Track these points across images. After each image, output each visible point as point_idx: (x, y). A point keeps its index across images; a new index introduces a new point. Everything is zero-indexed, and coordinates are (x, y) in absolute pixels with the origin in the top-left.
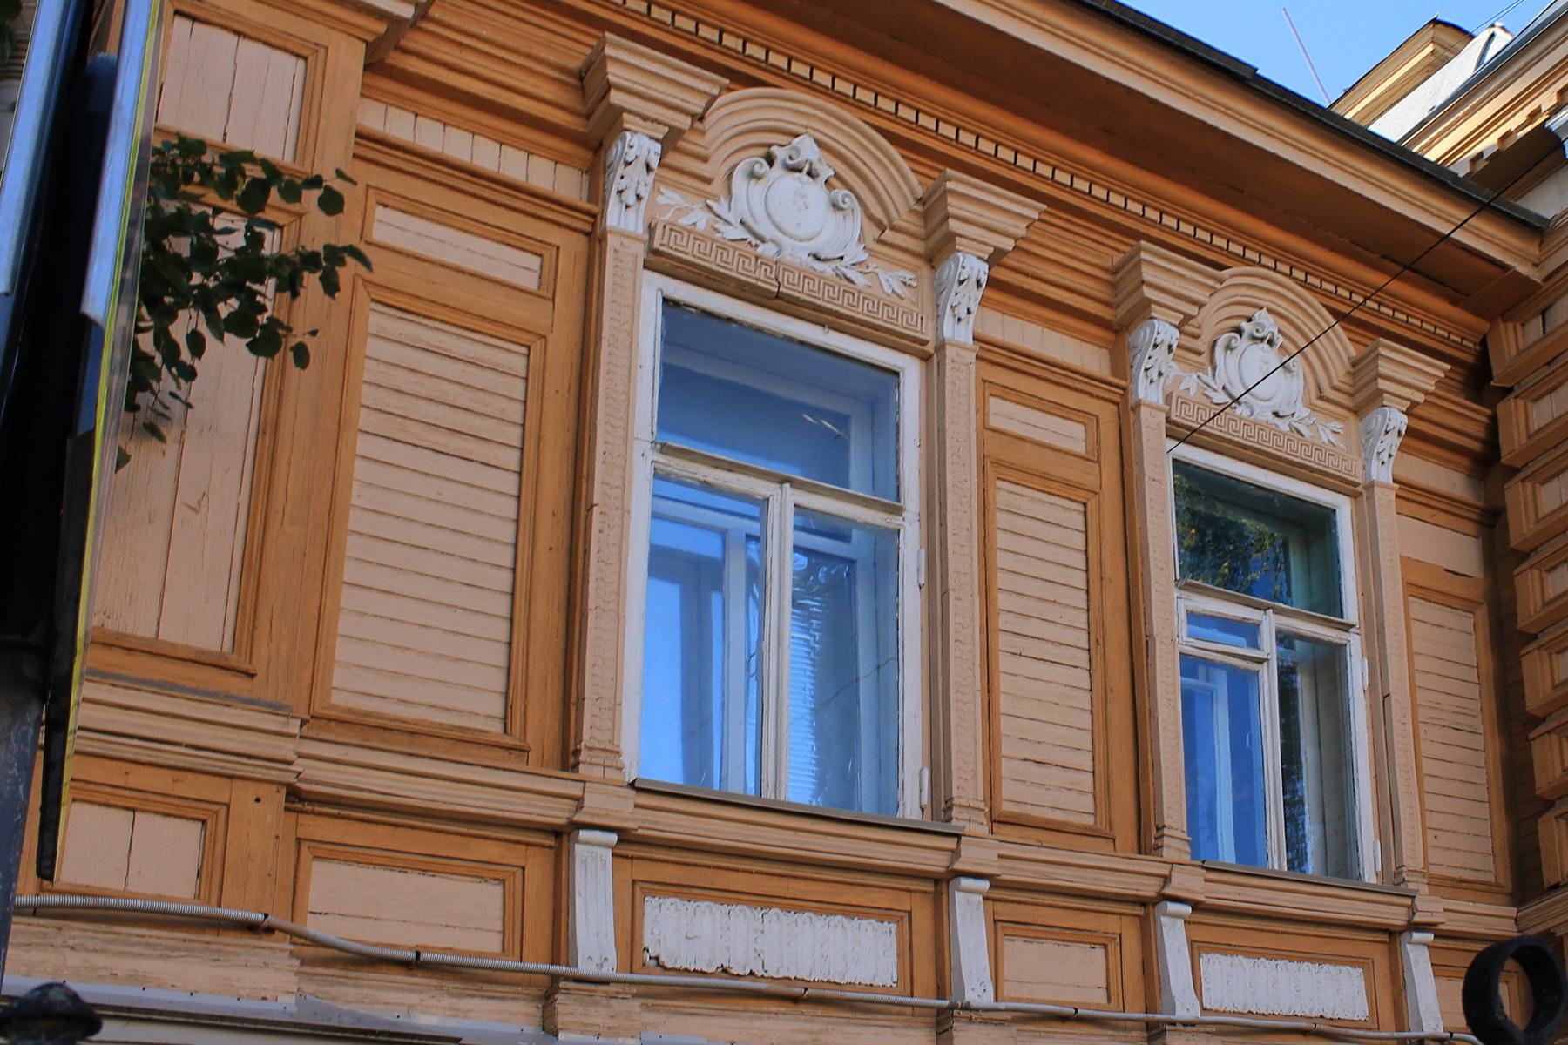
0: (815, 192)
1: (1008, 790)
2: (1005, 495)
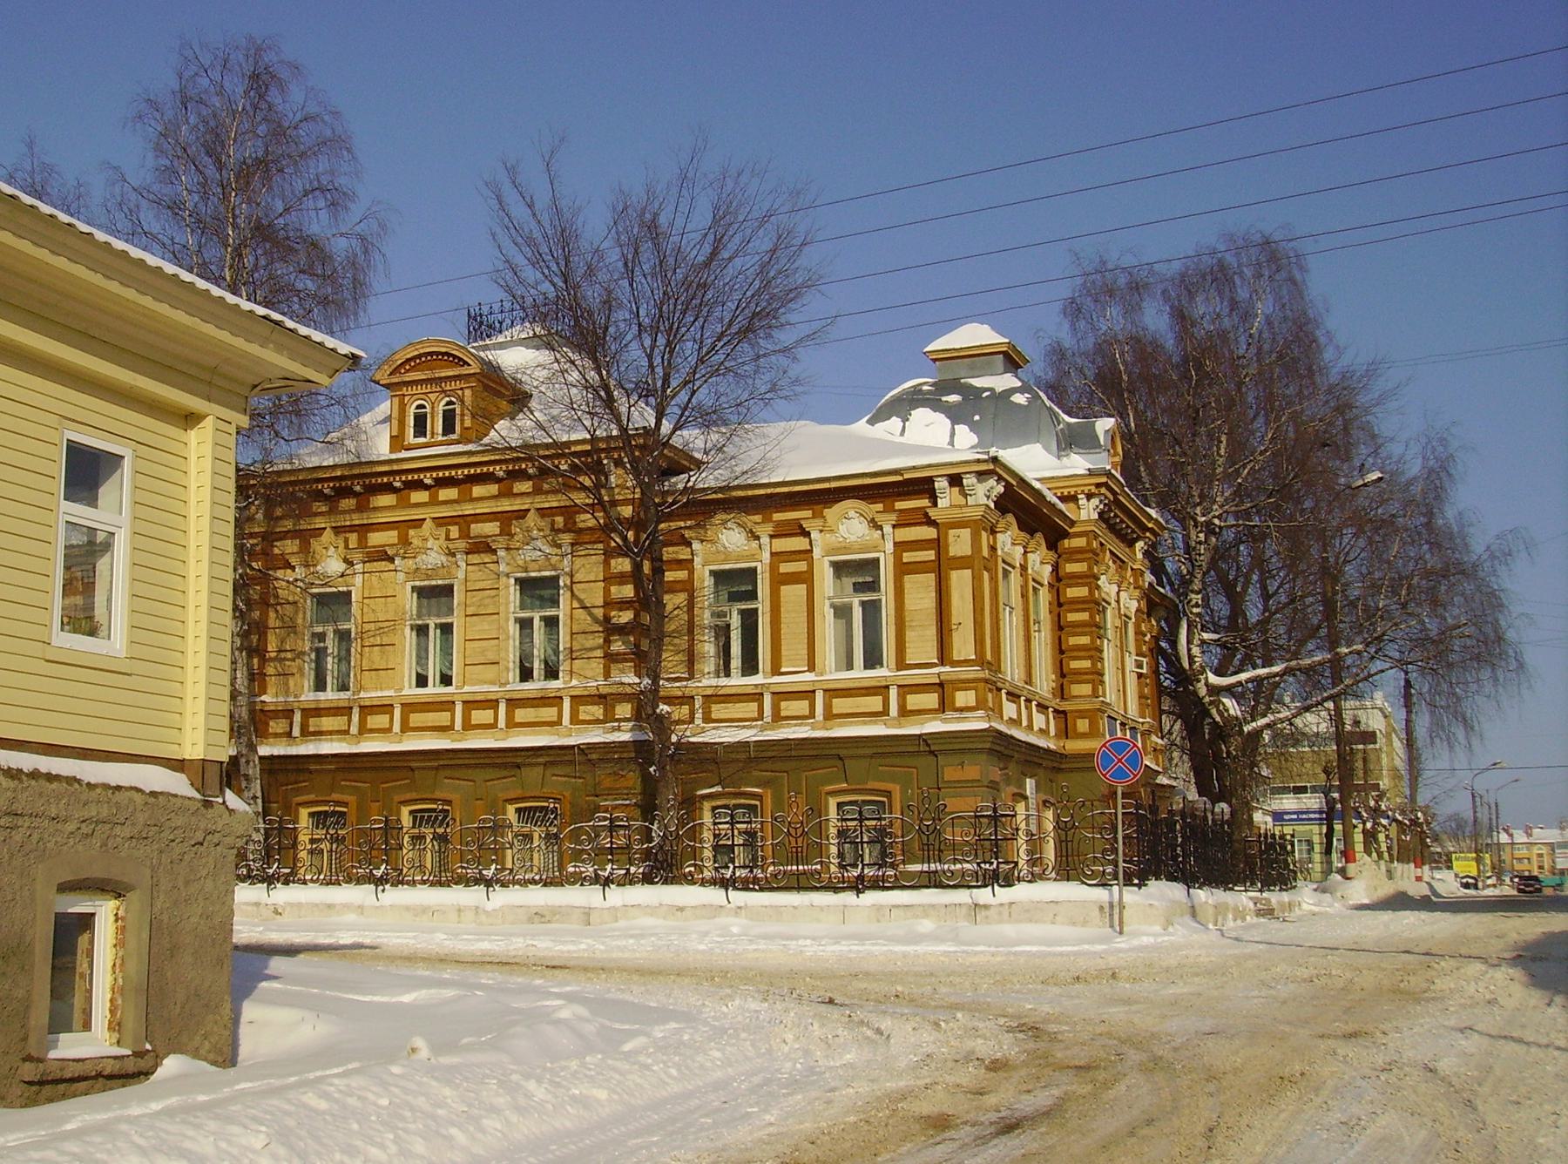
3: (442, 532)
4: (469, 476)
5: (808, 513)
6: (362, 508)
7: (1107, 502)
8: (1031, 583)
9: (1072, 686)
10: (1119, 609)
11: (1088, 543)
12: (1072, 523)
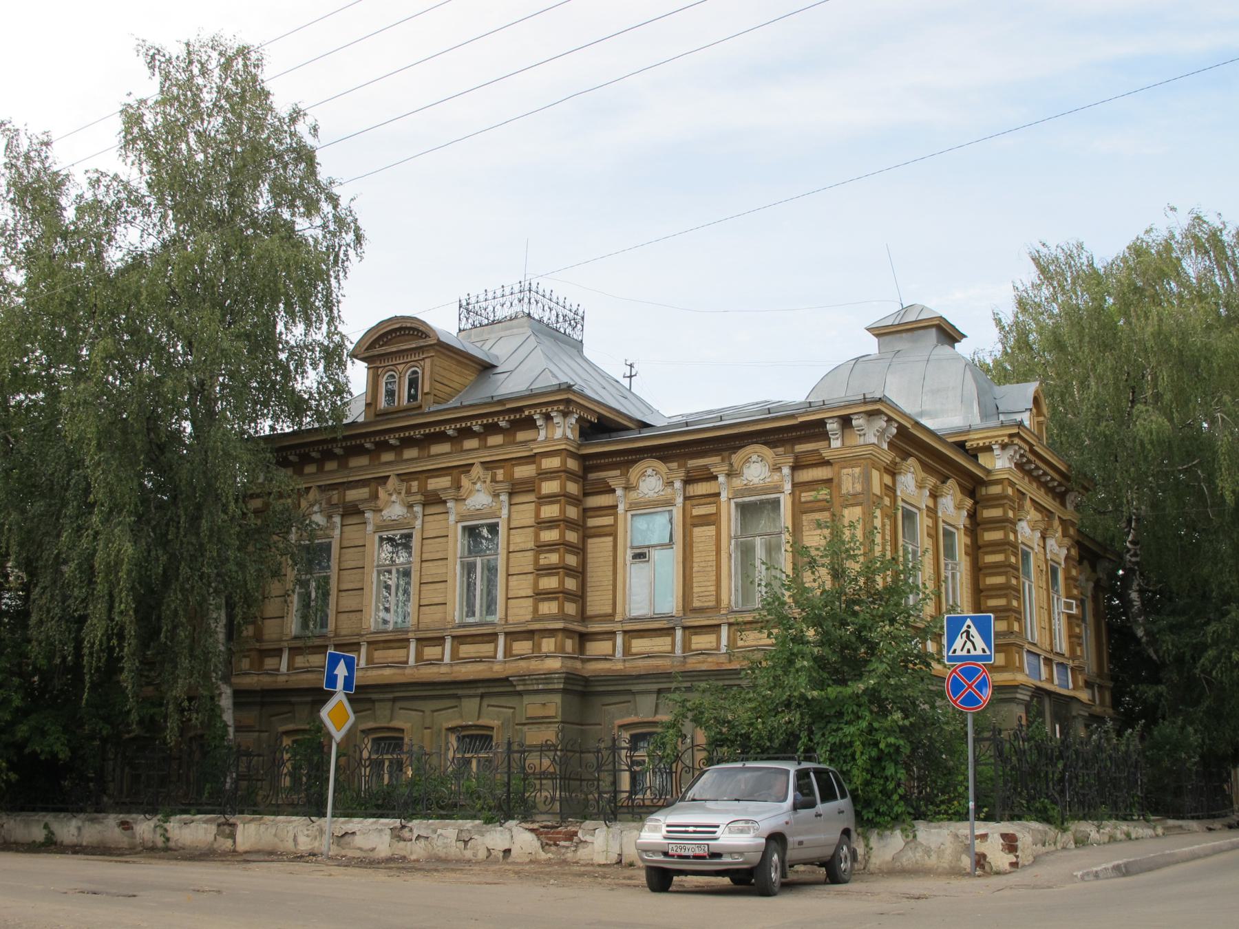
3: (404, 487)
4: (426, 435)
5: (717, 459)
6: (343, 465)
7: (1022, 452)
8: (941, 524)
9: (266, 637)
10: (1045, 554)
11: (1003, 489)
12: (988, 472)
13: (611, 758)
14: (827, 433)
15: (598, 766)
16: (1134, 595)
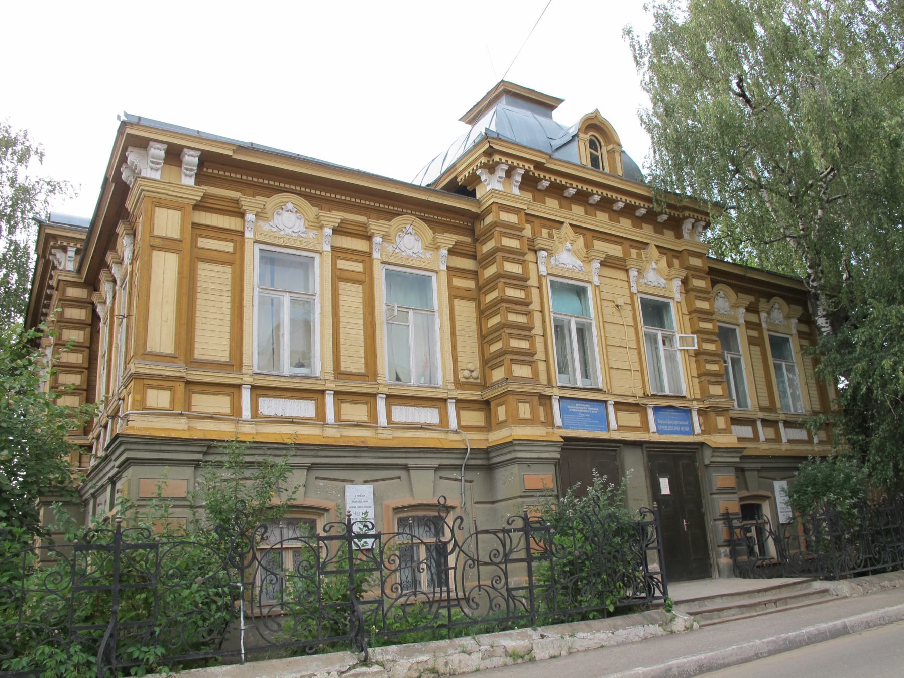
0: (293, 216)
1: (342, 364)
2: (342, 285)
13: (523, 544)
14: (181, 162)
15: (506, 555)
16: (821, 322)
